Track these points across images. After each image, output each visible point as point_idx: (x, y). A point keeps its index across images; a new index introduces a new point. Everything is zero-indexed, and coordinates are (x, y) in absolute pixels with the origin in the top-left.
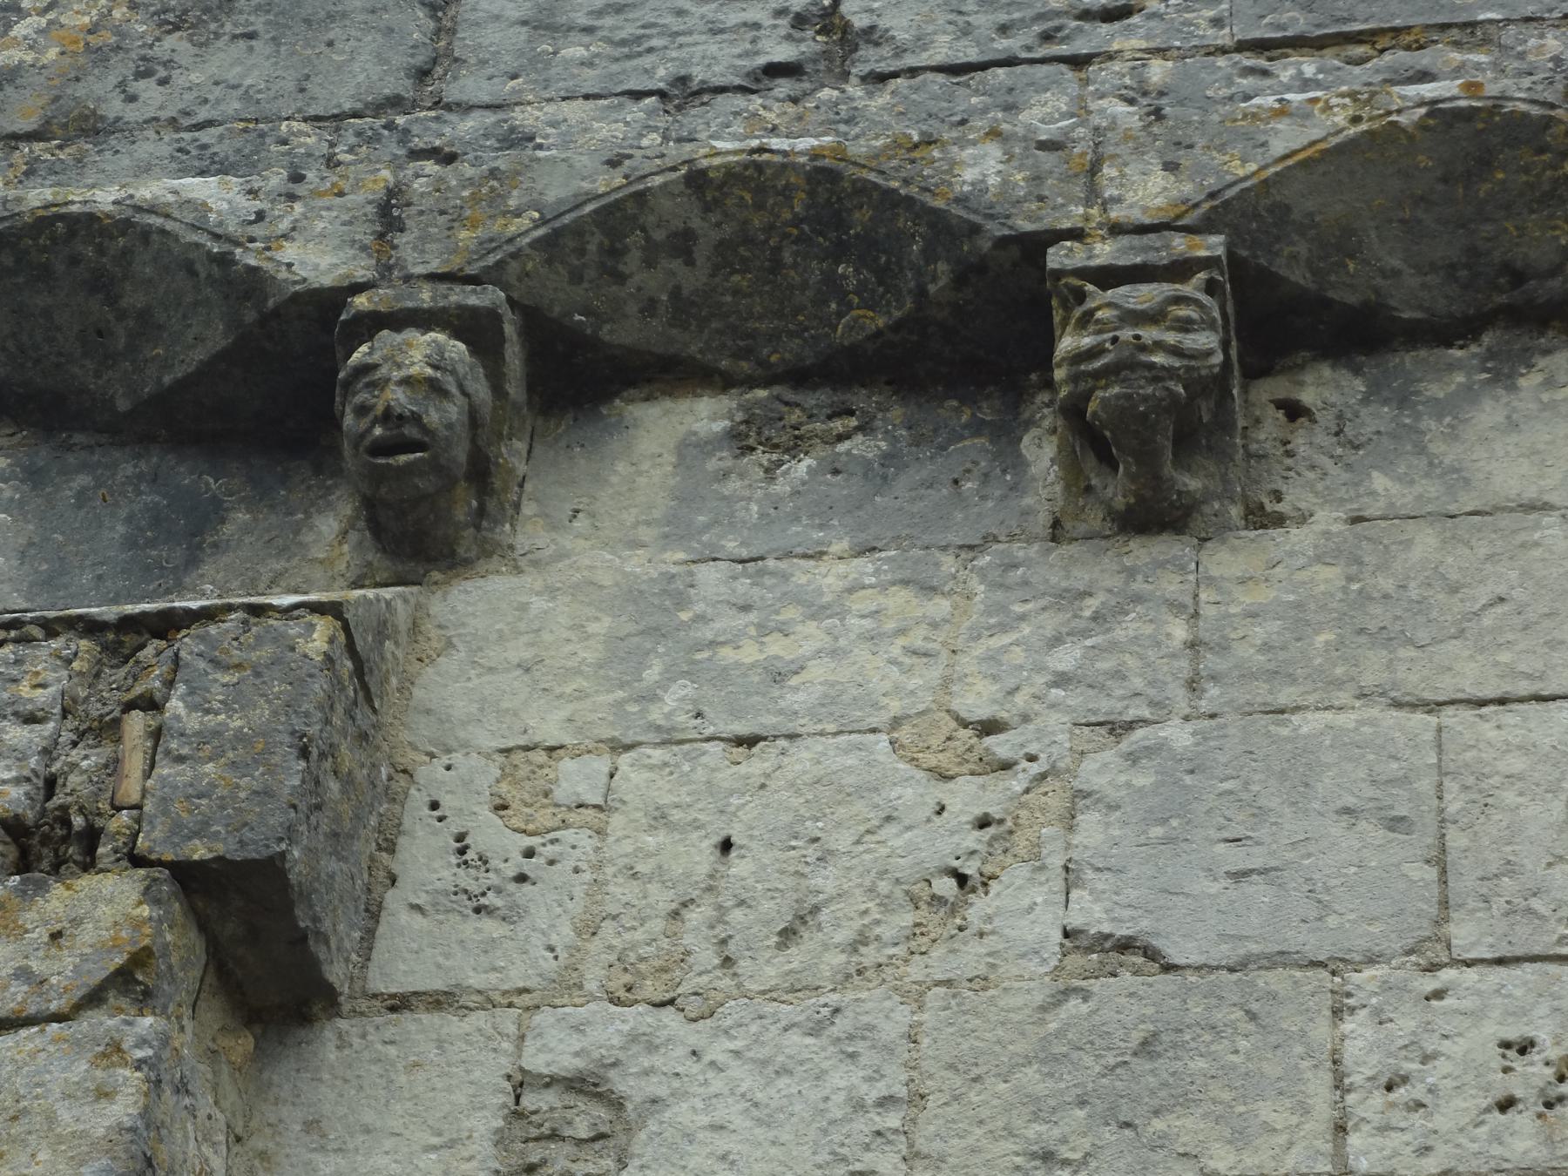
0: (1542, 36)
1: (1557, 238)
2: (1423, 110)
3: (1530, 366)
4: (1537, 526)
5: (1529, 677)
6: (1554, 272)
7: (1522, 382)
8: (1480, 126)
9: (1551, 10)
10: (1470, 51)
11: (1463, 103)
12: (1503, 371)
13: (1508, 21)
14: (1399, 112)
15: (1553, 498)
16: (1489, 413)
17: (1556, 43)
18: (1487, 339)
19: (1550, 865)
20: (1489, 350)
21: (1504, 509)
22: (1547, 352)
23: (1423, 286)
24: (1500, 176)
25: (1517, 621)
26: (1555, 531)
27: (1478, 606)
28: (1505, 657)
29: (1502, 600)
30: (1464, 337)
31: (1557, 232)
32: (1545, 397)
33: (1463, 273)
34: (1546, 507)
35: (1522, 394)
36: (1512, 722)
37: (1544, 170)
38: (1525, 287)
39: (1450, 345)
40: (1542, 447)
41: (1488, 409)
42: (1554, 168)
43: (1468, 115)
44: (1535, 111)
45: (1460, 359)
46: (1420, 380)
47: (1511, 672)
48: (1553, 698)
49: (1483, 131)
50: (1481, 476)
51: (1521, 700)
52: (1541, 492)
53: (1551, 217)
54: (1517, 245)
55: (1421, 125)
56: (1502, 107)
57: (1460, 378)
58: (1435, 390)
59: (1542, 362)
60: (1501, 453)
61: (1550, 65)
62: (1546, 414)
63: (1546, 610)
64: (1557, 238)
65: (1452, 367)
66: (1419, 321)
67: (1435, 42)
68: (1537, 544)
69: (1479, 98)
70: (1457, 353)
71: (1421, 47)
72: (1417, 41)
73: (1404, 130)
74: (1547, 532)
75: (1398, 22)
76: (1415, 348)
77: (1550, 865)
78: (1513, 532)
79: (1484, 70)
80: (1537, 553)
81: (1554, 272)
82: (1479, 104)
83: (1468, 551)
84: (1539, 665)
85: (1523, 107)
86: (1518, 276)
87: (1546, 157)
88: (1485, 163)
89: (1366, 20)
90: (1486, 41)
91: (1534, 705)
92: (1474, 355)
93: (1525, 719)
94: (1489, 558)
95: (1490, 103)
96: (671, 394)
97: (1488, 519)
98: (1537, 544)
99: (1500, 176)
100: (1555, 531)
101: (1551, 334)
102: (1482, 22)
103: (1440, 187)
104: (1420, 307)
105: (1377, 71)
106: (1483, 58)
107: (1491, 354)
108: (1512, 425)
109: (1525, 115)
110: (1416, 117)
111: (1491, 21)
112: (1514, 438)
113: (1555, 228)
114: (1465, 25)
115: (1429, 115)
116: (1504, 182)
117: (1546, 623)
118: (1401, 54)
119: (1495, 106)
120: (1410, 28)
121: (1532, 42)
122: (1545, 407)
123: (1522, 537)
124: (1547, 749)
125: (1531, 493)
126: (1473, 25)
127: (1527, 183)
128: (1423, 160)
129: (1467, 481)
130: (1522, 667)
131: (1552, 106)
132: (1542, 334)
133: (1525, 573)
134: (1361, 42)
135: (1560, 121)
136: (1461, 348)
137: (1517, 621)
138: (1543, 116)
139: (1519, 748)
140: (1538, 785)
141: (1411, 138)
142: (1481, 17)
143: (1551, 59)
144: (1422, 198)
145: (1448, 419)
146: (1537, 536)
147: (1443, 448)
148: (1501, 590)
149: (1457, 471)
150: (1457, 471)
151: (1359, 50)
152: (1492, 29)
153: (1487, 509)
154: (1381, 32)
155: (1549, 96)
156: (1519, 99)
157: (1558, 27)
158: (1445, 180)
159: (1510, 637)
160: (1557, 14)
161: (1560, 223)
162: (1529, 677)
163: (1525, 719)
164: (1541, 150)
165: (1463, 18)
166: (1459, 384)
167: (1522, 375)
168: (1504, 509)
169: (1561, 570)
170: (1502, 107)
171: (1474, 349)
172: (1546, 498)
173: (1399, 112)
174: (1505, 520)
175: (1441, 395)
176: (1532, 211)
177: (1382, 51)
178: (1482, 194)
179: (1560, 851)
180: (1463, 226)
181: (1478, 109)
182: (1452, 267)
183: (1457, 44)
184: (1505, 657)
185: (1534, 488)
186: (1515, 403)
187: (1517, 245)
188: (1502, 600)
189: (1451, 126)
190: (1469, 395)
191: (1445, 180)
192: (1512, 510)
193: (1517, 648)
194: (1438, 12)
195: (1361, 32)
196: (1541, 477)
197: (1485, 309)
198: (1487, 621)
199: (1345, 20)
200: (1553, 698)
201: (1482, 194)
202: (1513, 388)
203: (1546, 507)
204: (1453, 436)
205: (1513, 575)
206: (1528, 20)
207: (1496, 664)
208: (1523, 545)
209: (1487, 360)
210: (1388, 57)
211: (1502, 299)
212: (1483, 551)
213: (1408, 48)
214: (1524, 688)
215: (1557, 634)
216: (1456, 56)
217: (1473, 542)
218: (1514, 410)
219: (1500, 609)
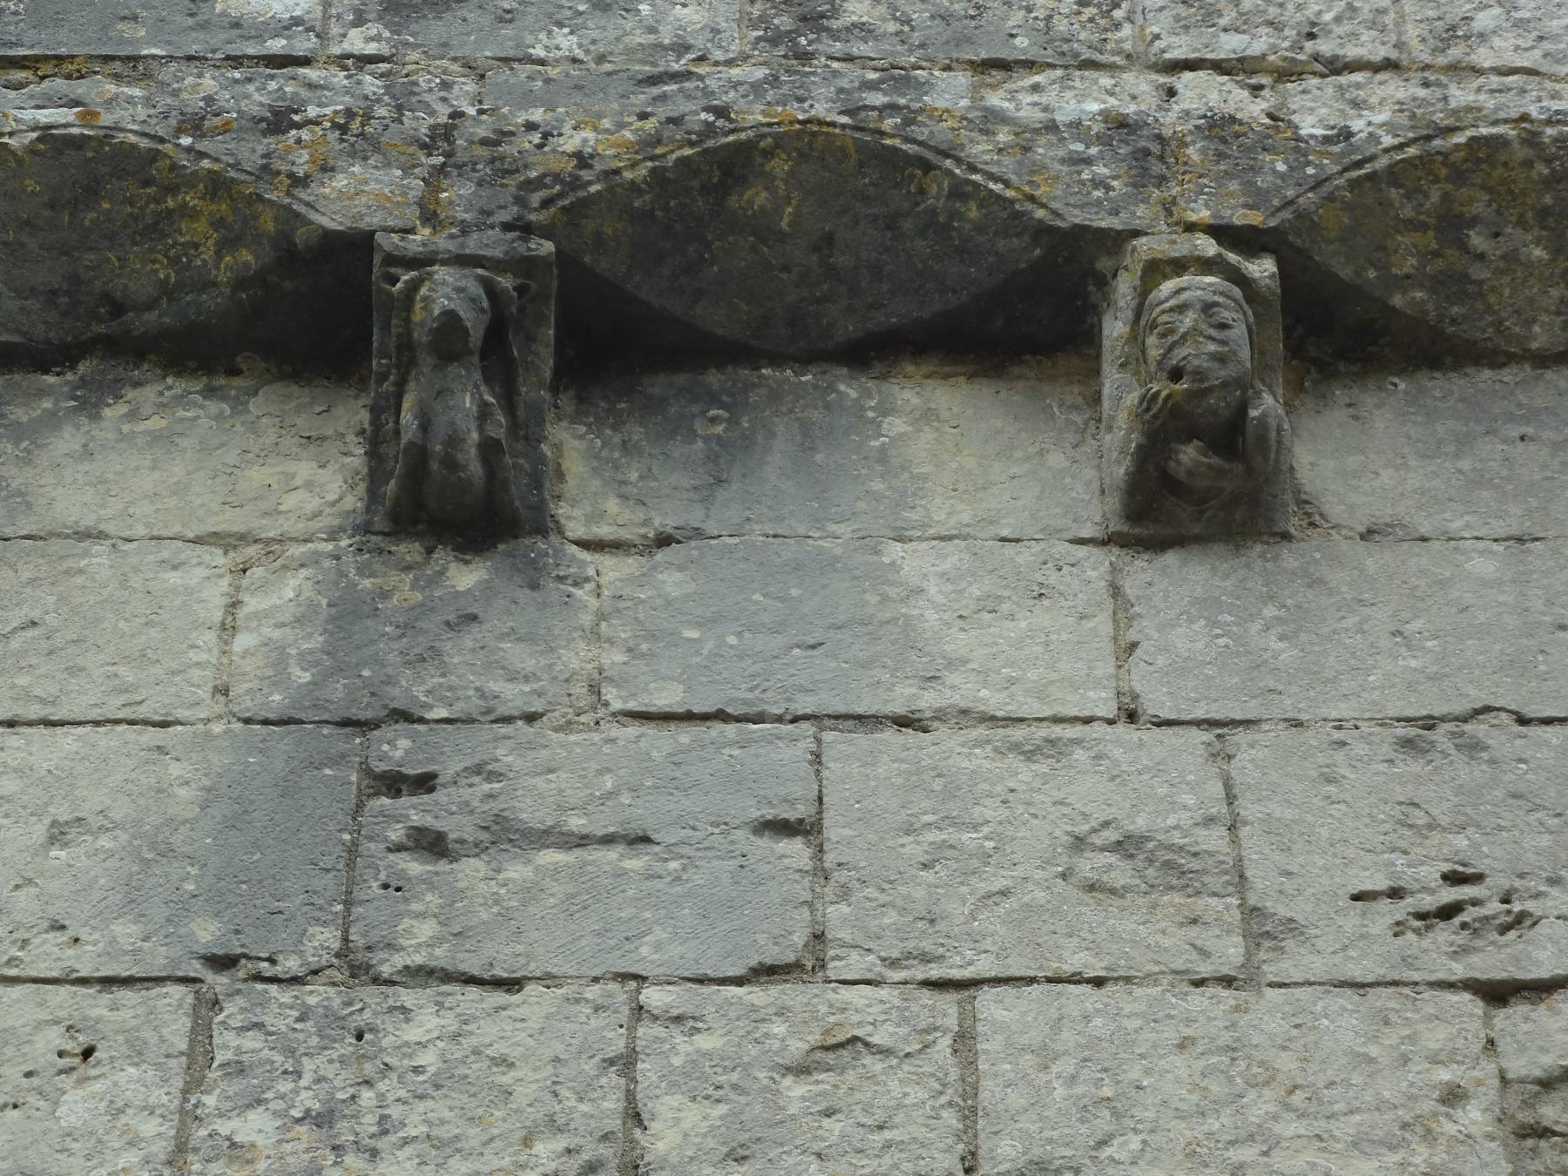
0: (200, 75)
1: (156, 271)
2: (35, 135)
3: (117, 397)
4: (86, 553)
5: (42, 701)
6: (152, 304)
7: (107, 412)
8: (90, 154)
9: (214, 51)
10: (129, 84)
11: (75, 131)
12: (89, 402)
13: (171, 58)
14: (11, 134)
15: (109, 528)
16: (67, 440)
17: (212, 82)
18: (82, 368)
19: (17, 887)
20: (82, 378)
21: (59, 535)
22: (138, 384)
23: (22, 309)
24: (106, 206)
25: (44, 645)
26: (104, 560)
27: (9, 629)
28: (23, 680)
29: (34, 624)
30: (62, 364)
31: (157, 266)
32: (126, 428)
33: (64, 300)
34: (101, 536)
35: (103, 424)
36: (16, 744)
37: (148, 203)
38: (124, 318)
39: (46, 371)
40: (110, 476)
41: (67, 436)
42: (158, 202)
43: (79, 143)
44: (144, 143)
45: (51, 386)
46: (8, 403)
47: (26, 695)
48: (62, 724)
49: (92, 159)
50: (43, 501)
51: (30, 724)
52: (99, 520)
53: (151, 250)
54: (118, 275)
55: (31, 150)
56: (113, 137)
57: (47, 404)
58: (21, 414)
59: (131, 394)
60: (70, 480)
61: (202, 104)
62: (123, 445)
63: (75, 637)
64: (156, 271)
65: (41, 393)
66: (15, 344)
67: (96, 73)
68: (81, 571)
69: (93, 128)
70: (51, 379)
71: (82, 77)
72: (78, 71)
73: (13, 153)
74: (95, 560)
75: (63, 51)
76: (10, 372)
77: (17, 887)
78: (61, 558)
79: (135, 104)
80: (80, 580)
81: (152, 304)
82: (91, 133)
83: (11, 574)
84: (54, 691)
85: (132, 138)
86: (117, 309)
87: (151, 190)
88: (92, 191)
89: (32, 46)
90: (147, 76)
91: (42, 729)
92: (67, 383)
93: (29, 743)
94: (31, 581)
95: (101, 133)
96: (971, 377)
97: (41, 543)
98: (81, 571)
99: (106, 206)
100: (104, 560)
101: (146, 366)
102: (145, 57)
103: (46, 213)
104: (17, 331)
105: (32, 97)
106: (136, 92)
107: (84, 383)
108: (87, 453)
109: (133, 146)
110: (26, 142)
111: (154, 57)
112: (86, 466)
113: (154, 261)
114: (129, 58)
115: (39, 139)
116: (109, 211)
117: (72, 649)
118: (59, 82)
119: (106, 136)
120: (73, 57)
121: (190, 80)
122: (123, 437)
123: (69, 563)
124: (44, 773)
125: (89, 521)
126: (134, 59)
127: (131, 215)
128: (31, 185)
129: (29, 506)
130: (37, 691)
131: (162, 140)
132: (137, 366)
133: (62, 599)
134: (25, 67)
135: (166, 155)
136: (58, 374)
137: (44, 645)
138: (150, 150)
139: (15, 770)
140: (24, 808)
141: (20, 161)
142: (145, 52)
143: (204, 98)
144: (28, 223)
145: (25, 444)
146: (83, 563)
147: (14, 471)
148: (35, 614)
149: (21, 494)
150: (21, 494)
151: (20, 75)
152: (154, 64)
153: (42, 534)
154: (46, 58)
155: (161, 131)
156: (131, 131)
157: (218, 67)
158: (51, 206)
159: (34, 661)
160: (219, 55)
161: (159, 256)
162: (42, 701)
163: (29, 743)
164: (147, 183)
165: (127, 51)
166: (45, 410)
167: (109, 405)
168: (59, 535)
169: (99, 598)
170: (113, 137)
171: (69, 376)
172: (102, 527)
173: (11, 134)
174: (55, 546)
175: (25, 419)
176: (134, 243)
177: (43, 78)
178: (87, 223)
179: (30, 874)
180: (66, 253)
181: (89, 137)
182: (54, 293)
183: (117, 77)
184: (23, 680)
185: (93, 517)
186: (95, 433)
187: (118, 275)
188: (34, 624)
189: (61, 152)
190: (53, 421)
191: (51, 206)
192: (67, 536)
193: (37, 672)
194: (104, 44)
195: (25, 57)
196: (102, 506)
197: (84, 338)
198: (15, 644)
199: (12, 45)
200: (62, 724)
201: (87, 223)
202: (96, 417)
203: (101, 536)
204: (26, 460)
205: (51, 600)
206: (190, 58)
207: (13, 687)
208: (66, 572)
209: (78, 388)
210: (46, 84)
211: (101, 329)
212: (26, 575)
213: (69, 77)
214: (35, 711)
215: (80, 661)
216: (111, 88)
217: (19, 566)
218: (93, 438)
219: (30, 633)
